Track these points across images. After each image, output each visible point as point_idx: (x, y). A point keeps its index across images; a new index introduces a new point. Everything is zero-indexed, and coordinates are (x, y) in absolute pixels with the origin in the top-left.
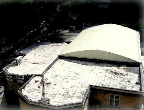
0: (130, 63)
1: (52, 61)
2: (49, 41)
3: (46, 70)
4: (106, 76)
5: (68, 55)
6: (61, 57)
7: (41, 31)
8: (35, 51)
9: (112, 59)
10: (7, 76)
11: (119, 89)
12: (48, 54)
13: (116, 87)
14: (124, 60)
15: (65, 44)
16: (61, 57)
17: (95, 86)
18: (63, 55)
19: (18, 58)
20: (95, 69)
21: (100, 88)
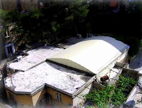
0: (88, 73)
1: (39, 63)
2: (53, 46)
3: (30, 68)
4: (23, 79)
5: (52, 60)
6: (48, 61)
7: (81, 35)
8: (38, 53)
9: (77, 68)
10: (7, 69)
11: (60, 90)
12: (43, 57)
13: (59, 87)
14: (85, 70)
15: (63, 49)
16: (48, 61)
17: (48, 85)
18: (49, 59)
19: (18, 57)
20: (62, 73)
21: (50, 86)
